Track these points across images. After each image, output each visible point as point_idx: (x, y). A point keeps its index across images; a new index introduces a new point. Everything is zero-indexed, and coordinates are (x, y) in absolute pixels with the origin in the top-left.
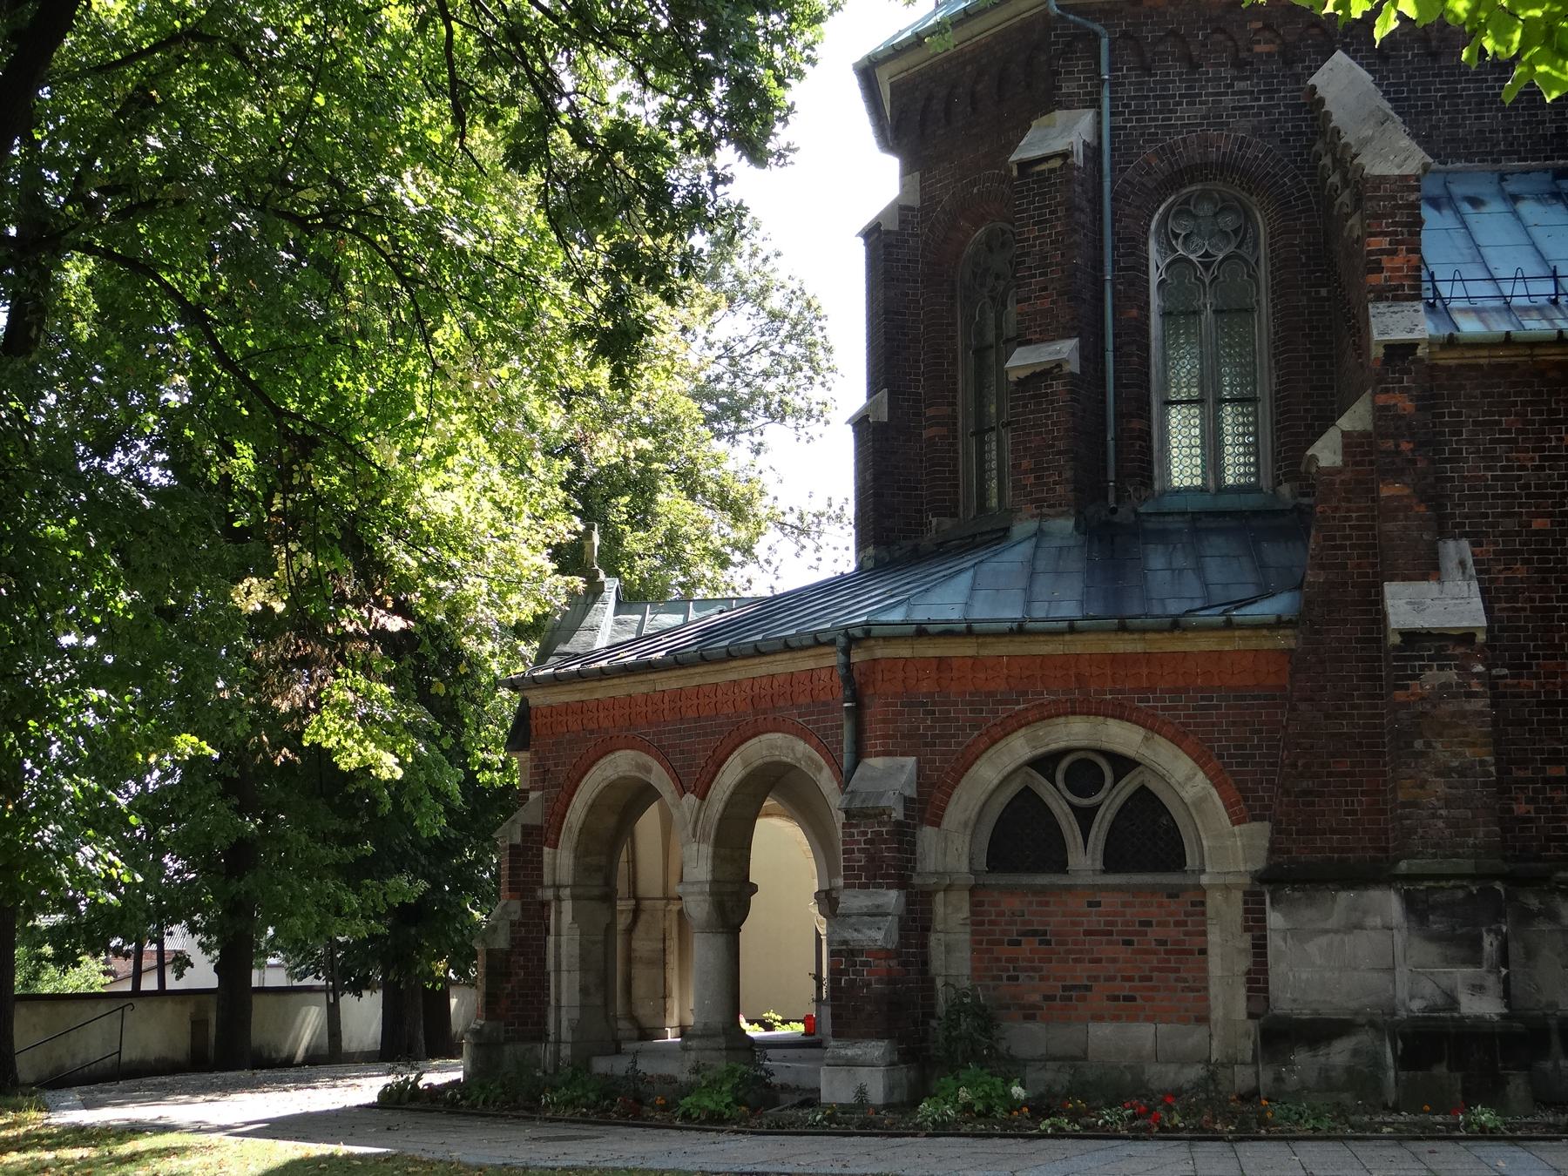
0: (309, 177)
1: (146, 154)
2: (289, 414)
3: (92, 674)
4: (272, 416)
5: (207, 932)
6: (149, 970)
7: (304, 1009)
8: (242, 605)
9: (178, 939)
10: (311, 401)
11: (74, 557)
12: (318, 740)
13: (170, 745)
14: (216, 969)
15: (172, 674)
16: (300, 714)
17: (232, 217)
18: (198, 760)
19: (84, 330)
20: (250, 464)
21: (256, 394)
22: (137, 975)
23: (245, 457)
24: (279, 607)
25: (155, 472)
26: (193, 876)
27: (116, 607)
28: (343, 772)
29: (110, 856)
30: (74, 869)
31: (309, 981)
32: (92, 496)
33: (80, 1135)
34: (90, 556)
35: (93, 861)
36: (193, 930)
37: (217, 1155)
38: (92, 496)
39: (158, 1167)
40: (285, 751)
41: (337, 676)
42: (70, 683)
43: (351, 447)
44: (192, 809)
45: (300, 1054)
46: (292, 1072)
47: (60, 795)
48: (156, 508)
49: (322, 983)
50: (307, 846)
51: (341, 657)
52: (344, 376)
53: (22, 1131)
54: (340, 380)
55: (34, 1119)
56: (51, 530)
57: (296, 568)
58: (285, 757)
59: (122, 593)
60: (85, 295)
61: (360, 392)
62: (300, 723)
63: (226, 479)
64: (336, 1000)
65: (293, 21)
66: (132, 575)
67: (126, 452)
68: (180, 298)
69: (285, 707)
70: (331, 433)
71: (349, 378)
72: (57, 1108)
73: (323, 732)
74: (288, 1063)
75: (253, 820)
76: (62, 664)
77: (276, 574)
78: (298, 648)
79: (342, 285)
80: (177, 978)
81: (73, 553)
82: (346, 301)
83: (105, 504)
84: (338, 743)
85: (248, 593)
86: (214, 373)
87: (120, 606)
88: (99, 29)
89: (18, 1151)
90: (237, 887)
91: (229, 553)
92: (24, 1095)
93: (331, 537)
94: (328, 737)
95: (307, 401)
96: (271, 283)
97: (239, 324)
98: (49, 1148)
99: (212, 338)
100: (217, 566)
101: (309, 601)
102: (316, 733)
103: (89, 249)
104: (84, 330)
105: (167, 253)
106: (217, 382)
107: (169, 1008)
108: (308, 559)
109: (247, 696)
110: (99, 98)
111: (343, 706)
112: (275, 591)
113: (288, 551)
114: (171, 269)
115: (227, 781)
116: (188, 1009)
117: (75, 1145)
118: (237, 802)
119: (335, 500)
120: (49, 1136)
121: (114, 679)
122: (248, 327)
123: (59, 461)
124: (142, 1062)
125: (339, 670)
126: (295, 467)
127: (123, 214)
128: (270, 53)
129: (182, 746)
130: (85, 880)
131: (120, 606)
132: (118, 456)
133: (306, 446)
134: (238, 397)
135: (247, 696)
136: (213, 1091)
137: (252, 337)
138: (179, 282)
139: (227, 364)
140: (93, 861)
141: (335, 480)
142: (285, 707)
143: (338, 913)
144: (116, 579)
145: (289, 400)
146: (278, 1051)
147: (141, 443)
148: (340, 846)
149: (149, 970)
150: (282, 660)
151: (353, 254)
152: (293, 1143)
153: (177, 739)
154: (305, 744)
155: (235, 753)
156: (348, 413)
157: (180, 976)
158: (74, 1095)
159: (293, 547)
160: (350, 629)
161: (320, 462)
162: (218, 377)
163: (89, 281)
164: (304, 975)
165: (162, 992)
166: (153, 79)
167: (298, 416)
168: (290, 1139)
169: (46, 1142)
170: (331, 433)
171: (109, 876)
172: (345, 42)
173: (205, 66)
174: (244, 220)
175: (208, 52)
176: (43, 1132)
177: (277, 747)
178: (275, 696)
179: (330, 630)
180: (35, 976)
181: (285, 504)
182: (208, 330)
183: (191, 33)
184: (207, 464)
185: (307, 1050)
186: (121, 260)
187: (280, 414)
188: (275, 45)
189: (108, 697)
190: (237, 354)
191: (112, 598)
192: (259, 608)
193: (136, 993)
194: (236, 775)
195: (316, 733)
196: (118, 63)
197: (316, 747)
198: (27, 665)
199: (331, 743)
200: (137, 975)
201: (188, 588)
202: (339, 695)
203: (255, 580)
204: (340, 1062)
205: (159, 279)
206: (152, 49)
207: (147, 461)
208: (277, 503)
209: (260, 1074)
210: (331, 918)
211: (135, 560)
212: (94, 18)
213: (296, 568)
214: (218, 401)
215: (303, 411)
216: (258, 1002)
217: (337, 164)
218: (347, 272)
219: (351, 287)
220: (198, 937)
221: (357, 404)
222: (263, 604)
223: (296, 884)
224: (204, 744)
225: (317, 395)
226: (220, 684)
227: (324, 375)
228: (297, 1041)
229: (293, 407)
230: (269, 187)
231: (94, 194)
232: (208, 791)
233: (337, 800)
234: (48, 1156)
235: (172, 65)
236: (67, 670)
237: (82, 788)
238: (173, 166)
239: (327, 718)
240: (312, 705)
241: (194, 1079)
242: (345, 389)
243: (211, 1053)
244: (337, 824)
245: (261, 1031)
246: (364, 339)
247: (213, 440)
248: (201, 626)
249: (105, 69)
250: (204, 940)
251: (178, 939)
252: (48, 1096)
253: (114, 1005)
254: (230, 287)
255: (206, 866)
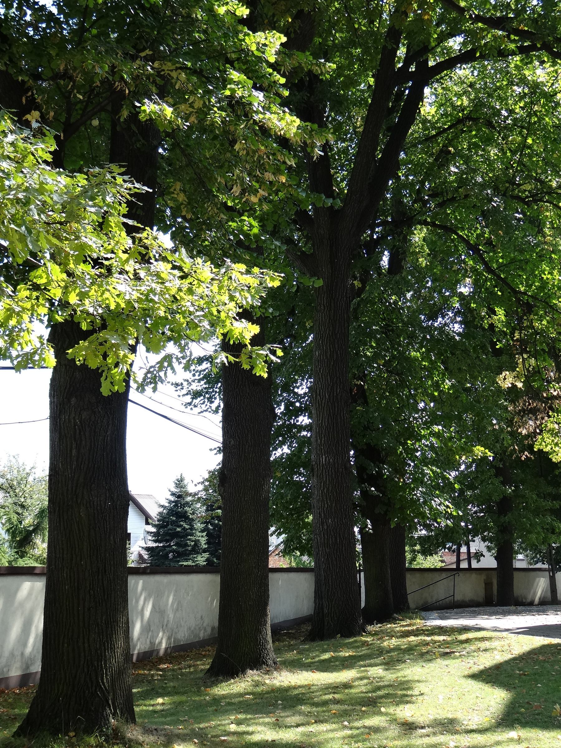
0: (525, 178)
1: (450, 175)
2: (520, 292)
3: (435, 420)
4: (512, 294)
5: (491, 540)
6: (464, 560)
7: (537, 579)
8: (502, 385)
9: (477, 545)
10: (531, 285)
11: (425, 365)
12: (541, 447)
13: (472, 451)
14: (496, 558)
15: (468, 417)
16: (532, 435)
17: (491, 200)
18: (484, 458)
19: (423, 262)
20: (503, 318)
21: (504, 284)
22: (458, 561)
23: (501, 314)
24: (520, 385)
25: (457, 326)
26: (482, 514)
27: (444, 388)
28: (554, 463)
29: (447, 503)
30: (431, 508)
31: (539, 565)
32: (432, 336)
33: (442, 630)
34: (432, 364)
35: (439, 505)
36: (484, 539)
37: (507, 642)
38: (432, 336)
39: (479, 645)
40: (526, 453)
41: (549, 417)
42: (425, 423)
43: (551, 307)
44: (482, 482)
45: (537, 600)
46: (535, 608)
47: (424, 475)
48: (461, 340)
49: (546, 566)
50: (536, 500)
51: (551, 408)
52: (546, 273)
53: (415, 628)
54: (545, 274)
55: (419, 623)
56: (413, 354)
57: (527, 366)
58: (526, 456)
59: (447, 381)
60: (423, 246)
61: (554, 279)
62: (532, 441)
63: (492, 326)
64: (554, 574)
65: (515, 105)
66: (449, 372)
67: (443, 317)
68: (467, 242)
69: (524, 432)
70: (541, 300)
71: (549, 273)
72: (428, 619)
73: (544, 443)
74: (531, 604)
75: (510, 488)
76: (422, 414)
77: (517, 369)
78: (530, 404)
79: (542, 230)
80: (478, 562)
81: (424, 363)
82: (545, 237)
83: (438, 339)
84: (552, 449)
85: (505, 379)
86: (485, 276)
87: (446, 387)
88: (425, 121)
89: (414, 636)
90: (503, 519)
91: (494, 361)
92: (413, 613)
93: (543, 350)
94: (546, 446)
95: (530, 286)
96: (509, 229)
97: (495, 252)
98: (428, 635)
99: (483, 259)
100: (488, 368)
101: (534, 381)
102: (541, 445)
103: (425, 223)
104: (423, 262)
105: (460, 221)
106: (486, 280)
107: (474, 576)
108: (533, 361)
109: (507, 427)
110: (426, 153)
111: (553, 431)
112: (517, 377)
113: (523, 358)
114: (463, 229)
115: (498, 469)
116: (483, 577)
117: (439, 635)
118: (502, 479)
119: (545, 332)
120: (427, 630)
121: (446, 420)
122: (500, 253)
123: (413, 321)
124: (463, 601)
125: (550, 414)
126: (525, 318)
127: (440, 205)
128: (505, 122)
129: (477, 452)
130: (436, 515)
131: (446, 387)
132: (440, 319)
133: (529, 308)
134: (496, 286)
135: (507, 427)
136: (499, 615)
137: (502, 257)
138: (466, 235)
139: (489, 269)
140: (439, 505)
141: (545, 322)
142: (524, 432)
143: (553, 532)
144: (444, 375)
145: (520, 286)
146: (526, 599)
147: (450, 313)
148: (552, 500)
149: (464, 560)
150: (523, 410)
151: (548, 214)
152: (542, 637)
153: (475, 449)
154: (535, 450)
155: (501, 455)
156: (549, 290)
157: (479, 561)
158: (435, 614)
159: (525, 356)
160: (555, 394)
161: (537, 314)
162: (486, 277)
163: (424, 239)
164: (537, 562)
165: (470, 569)
166: (450, 142)
167: (525, 293)
168: (540, 636)
169: (426, 633)
170: (541, 300)
171: (447, 512)
172: (541, 111)
173: (474, 133)
174: (497, 201)
175: (476, 125)
176: (424, 628)
177: (522, 451)
178: (520, 427)
179: (545, 395)
180: (414, 559)
181: (520, 336)
182: (481, 256)
183: (468, 118)
184: (482, 319)
185: (540, 599)
186: (440, 227)
187: (516, 293)
188: (506, 118)
189: (443, 430)
190: (495, 266)
191: (443, 383)
192: (510, 386)
193: (458, 569)
194: (501, 466)
195: (541, 445)
196: (434, 136)
197: (540, 451)
198: (406, 415)
199: (548, 449)
200: (458, 561)
201: (476, 378)
202: (550, 426)
203: (507, 373)
204: (557, 604)
205: (457, 234)
206: (450, 128)
207: (453, 321)
208: (517, 336)
209: (520, 608)
210: (550, 535)
211: (451, 366)
212: (74, 158)
213: (527, 366)
214: (487, 289)
215: (527, 291)
216: (516, 575)
217: (539, 171)
218: (545, 223)
219: (547, 231)
220: (486, 543)
221: (553, 285)
222: (512, 384)
223: (532, 518)
224: (487, 451)
225: (534, 282)
226: (494, 422)
227: (537, 272)
228: (535, 594)
229: (522, 289)
230: (507, 185)
231: (426, 198)
232: (489, 474)
233: (549, 478)
234: (428, 639)
235: (459, 134)
236: (424, 417)
237: (433, 472)
238: (461, 181)
239: (545, 437)
240: (538, 431)
241: (488, 609)
242: (547, 279)
243: (495, 598)
244: (550, 489)
245: (518, 589)
246: (555, 254)
247: (485, 306)
248: (483, 396)
249: (429, 139)
250: (489, 544)
251: (477, 545)
252: (423, 614)
253: (449, 574)
254: (490, 235)
255: (489, 510)
